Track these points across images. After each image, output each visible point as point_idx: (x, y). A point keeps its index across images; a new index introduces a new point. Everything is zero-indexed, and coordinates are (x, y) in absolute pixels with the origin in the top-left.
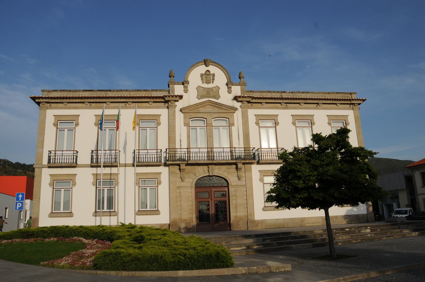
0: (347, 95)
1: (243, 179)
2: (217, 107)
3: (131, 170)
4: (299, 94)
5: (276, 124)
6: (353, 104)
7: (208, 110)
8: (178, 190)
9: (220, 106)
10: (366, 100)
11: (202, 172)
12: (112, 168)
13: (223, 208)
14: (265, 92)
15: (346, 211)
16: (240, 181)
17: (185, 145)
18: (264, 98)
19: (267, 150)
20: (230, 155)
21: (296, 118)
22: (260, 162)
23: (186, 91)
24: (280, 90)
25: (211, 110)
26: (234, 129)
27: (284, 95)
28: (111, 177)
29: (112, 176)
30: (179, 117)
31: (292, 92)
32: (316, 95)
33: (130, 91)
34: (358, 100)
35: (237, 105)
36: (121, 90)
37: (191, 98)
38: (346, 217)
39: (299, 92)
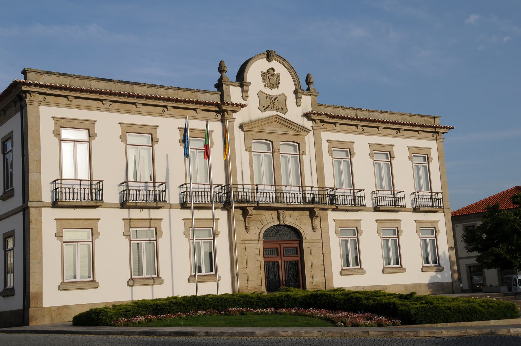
0: (429, 119)
1: (318, 230)
2: (286, 126)
3: (180, 215)
4: (376, 114)
5: (91, 136)
6: (438, 133)
7: (275, 129)
8: (242, 245)
9: (288, 124)
10: (453, 128)
11: (270, 219)
12: (151, 210)
13: (297, 273)
14: (339, 107)
15: (429, 278)
16: (314, 233)
17: (248, 181)
18: (172, 100)
19: (72, 182)
20: (274, 196)
21: (127, 129)
22: (60, 203)
23: (245, 97)
24: (355, 107)
25: (278, 129)
26: (306, 159)
27: (361, 115)
28: (150, 225)
29: (152, 223)
30: (239, 136)
31: (369, 111)
32: (395, 116)
33: (168, 88)
34: (444, 127)
35: (308, 124)
36: (155, 86)
37: (252, 111)
38: (431, 285)
39: (376, 111)
